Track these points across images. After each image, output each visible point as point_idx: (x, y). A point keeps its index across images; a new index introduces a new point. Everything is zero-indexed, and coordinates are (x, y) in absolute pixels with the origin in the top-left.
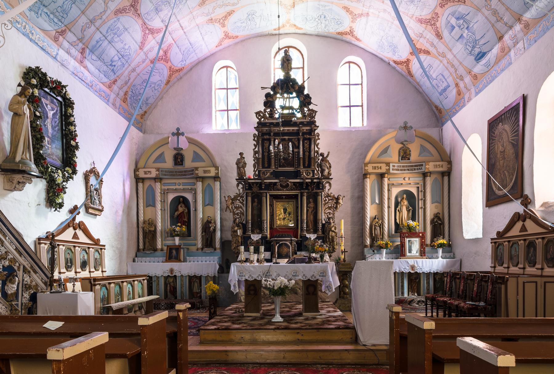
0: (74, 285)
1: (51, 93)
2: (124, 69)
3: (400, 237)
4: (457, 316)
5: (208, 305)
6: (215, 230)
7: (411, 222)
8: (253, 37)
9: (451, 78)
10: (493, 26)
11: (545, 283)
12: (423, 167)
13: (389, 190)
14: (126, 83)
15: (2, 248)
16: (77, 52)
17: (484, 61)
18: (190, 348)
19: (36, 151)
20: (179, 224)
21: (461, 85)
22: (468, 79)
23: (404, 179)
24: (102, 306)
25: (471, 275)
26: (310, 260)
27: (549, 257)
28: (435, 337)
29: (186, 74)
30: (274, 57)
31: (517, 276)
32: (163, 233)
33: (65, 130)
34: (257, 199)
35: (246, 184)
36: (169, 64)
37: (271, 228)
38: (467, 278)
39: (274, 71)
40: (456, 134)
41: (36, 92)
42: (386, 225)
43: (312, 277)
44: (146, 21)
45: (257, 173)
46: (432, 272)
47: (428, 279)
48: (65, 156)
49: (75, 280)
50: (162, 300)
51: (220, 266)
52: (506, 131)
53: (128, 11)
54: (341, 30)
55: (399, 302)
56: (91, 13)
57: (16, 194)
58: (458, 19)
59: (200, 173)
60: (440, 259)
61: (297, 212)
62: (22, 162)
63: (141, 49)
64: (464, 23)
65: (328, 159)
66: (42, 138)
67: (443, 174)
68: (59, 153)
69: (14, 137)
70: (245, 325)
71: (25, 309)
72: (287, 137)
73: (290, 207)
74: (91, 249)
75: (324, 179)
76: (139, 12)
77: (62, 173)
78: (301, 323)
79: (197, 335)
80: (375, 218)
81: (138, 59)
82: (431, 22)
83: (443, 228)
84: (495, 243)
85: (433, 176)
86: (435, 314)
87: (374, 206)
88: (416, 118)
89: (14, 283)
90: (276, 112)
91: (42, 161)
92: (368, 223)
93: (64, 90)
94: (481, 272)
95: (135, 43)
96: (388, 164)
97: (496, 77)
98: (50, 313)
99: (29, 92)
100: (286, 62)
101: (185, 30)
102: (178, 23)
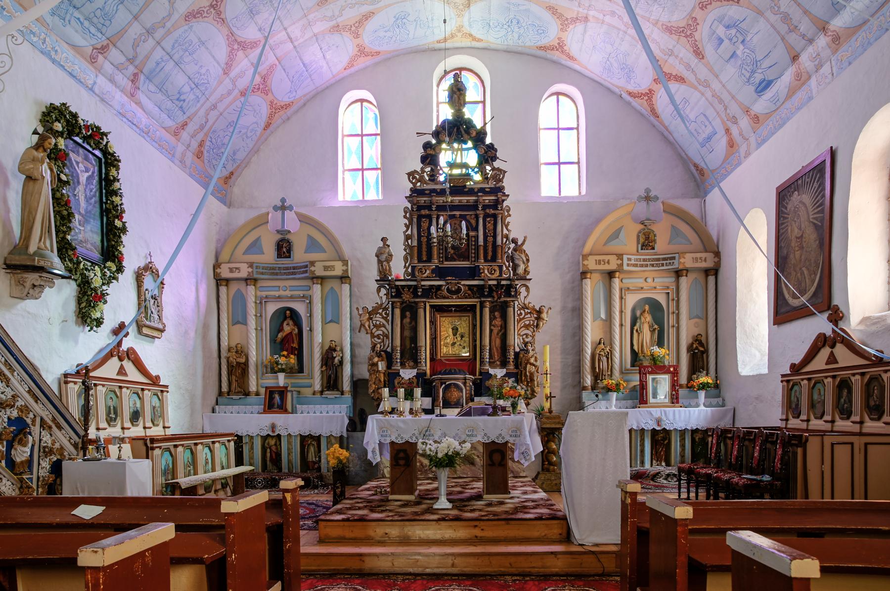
0: (120, 449)
1: (85, 145)
2: (199, 105)
3: (640, 373)
4: (727, 497)
5: (332, 482)
6: (341, 363)
7: (656, 349)
8: (404, 54)
9: (718, 120)
10: (783, 39)
11: (866, 444)
12: (676, 262)
13: (621, 298)
14: (202, 127)
15: (8, 390)
16: (125, 79)
17: (769, 94)
18: (303, 550)
19: (61, 235)
20: (285, 353)
21: (735, 131)
22: (744, 122)
23: (646, 280)
24: (164, 482)
25: (749, 433)
26: (496, 411)
27: (872, 403)
28: (693, 532)
29: (296, 112)
30: (438, 85)
31: (821, 434)
32: (260, 367)
33: (106, 203)
34: (410, 311)
35: (391, 288)
36: (270, 97)
37: (432, 359)
38: (744, 439)
39: (438, 106)
40: (728, 207)
41: (62, 143)
42: (617, 355)
43: (498, 438)
44: (234, 29)
45: (410, 270)
46: (689, 428)
47: (683, 439)
48: (105, 244)
49: (122, 440)
50: (259, 474)
51: (350, 419)
52: (804, 204)
53: (205, 14)
54: (544, 42)
55: (637, 477)
56: (148, 19)
57: (29, 304)
58: (728, 27)
59: (319, 271)
60: (702, 407)
61: (474, 334)
62: (39, 253)
63: (225, 73)
64: (738, 35)
65: (524, 247)
66: (70, 215)
67: (707, 272)
68: (97, 239)
69: (26, 214)
70: (390, 514)
71: (43, 486)
72: (457, 213)
73: (463, 325)
74: (146, 392)
75: (517, 279)
76: (223, 16)
77: (101, 271)
78: (480, 510)
79: (315, 529)
80: (600, 343)
81: (222, 90)
82: (686, 31)
83: (704, 359)
84: (788, 381)
85: (692, 276)
86: (692, 495)
87: (598, 322)
88: (666, 185)
89: (25, 445)
90: (441, 172)
91: (70, 253)
92: (589, 351)
93: (105, 140)
94: (765, 428)
95: (216, 65)
96: (620, 256)
97: (788, 119)
98: (83, 492)
99: (50, 144)
100: (457, 93)
101: (296, 44)
102: (284, 33)
